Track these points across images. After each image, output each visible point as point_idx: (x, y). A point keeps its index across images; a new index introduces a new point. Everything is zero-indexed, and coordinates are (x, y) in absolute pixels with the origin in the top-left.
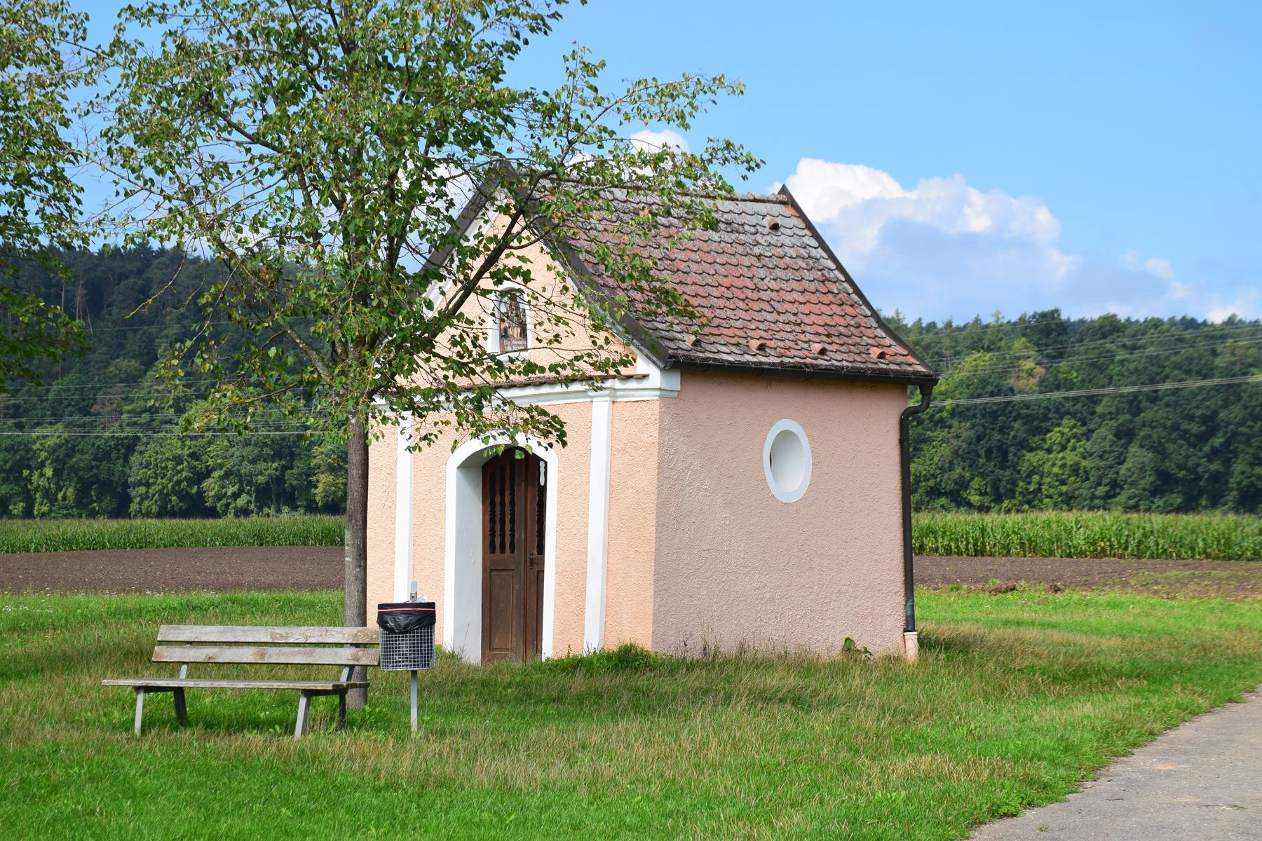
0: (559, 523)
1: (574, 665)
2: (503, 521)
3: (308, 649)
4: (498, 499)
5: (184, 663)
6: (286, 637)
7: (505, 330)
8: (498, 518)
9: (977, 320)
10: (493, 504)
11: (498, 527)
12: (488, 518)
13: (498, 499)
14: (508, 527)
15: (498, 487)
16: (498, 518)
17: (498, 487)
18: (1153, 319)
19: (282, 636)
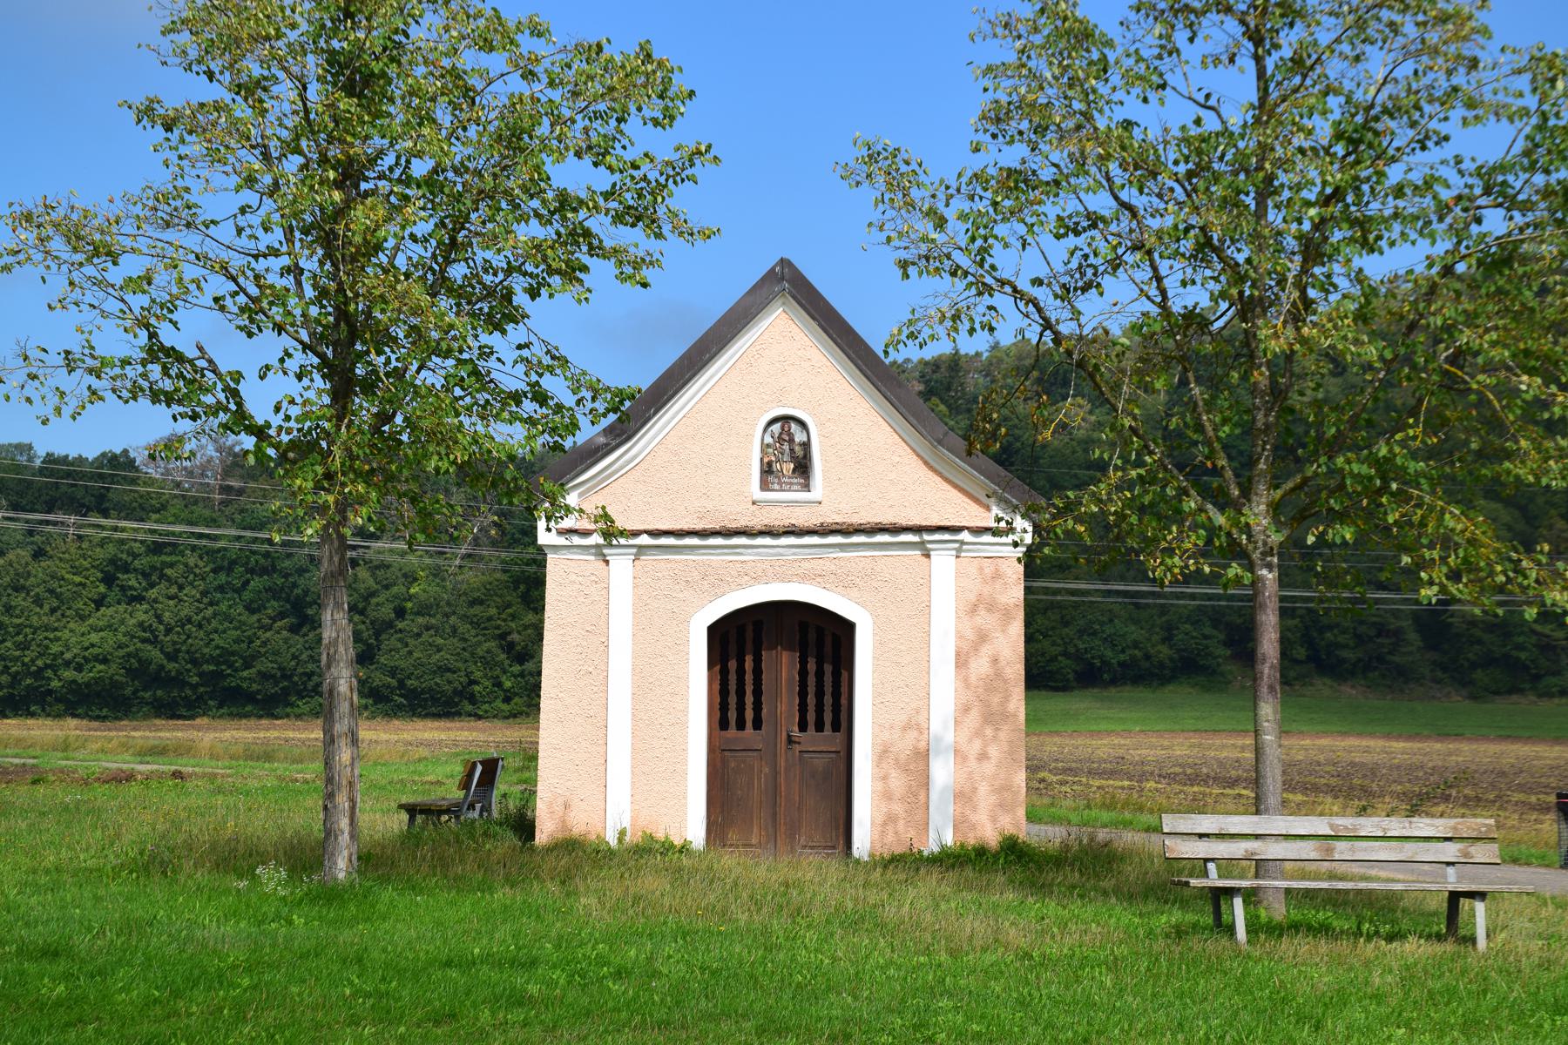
0: (877, 694)
1: (905, 863)
2: (820, 694)
3: (1394, 844)
4: (733, 665)
5: (1212, 860)
6: (1355, 830)
7: (770, 464)
8: (733, 687)
9: (125, 452)
10: (724, 673)
11: (733, 700)
12: (717, 687)
13: (733, 665)
14: (749, 699)
15: (733, 648)
16: (733, 687)
17: (733, 648)
18: (104, 455)
19: (1346, 828)
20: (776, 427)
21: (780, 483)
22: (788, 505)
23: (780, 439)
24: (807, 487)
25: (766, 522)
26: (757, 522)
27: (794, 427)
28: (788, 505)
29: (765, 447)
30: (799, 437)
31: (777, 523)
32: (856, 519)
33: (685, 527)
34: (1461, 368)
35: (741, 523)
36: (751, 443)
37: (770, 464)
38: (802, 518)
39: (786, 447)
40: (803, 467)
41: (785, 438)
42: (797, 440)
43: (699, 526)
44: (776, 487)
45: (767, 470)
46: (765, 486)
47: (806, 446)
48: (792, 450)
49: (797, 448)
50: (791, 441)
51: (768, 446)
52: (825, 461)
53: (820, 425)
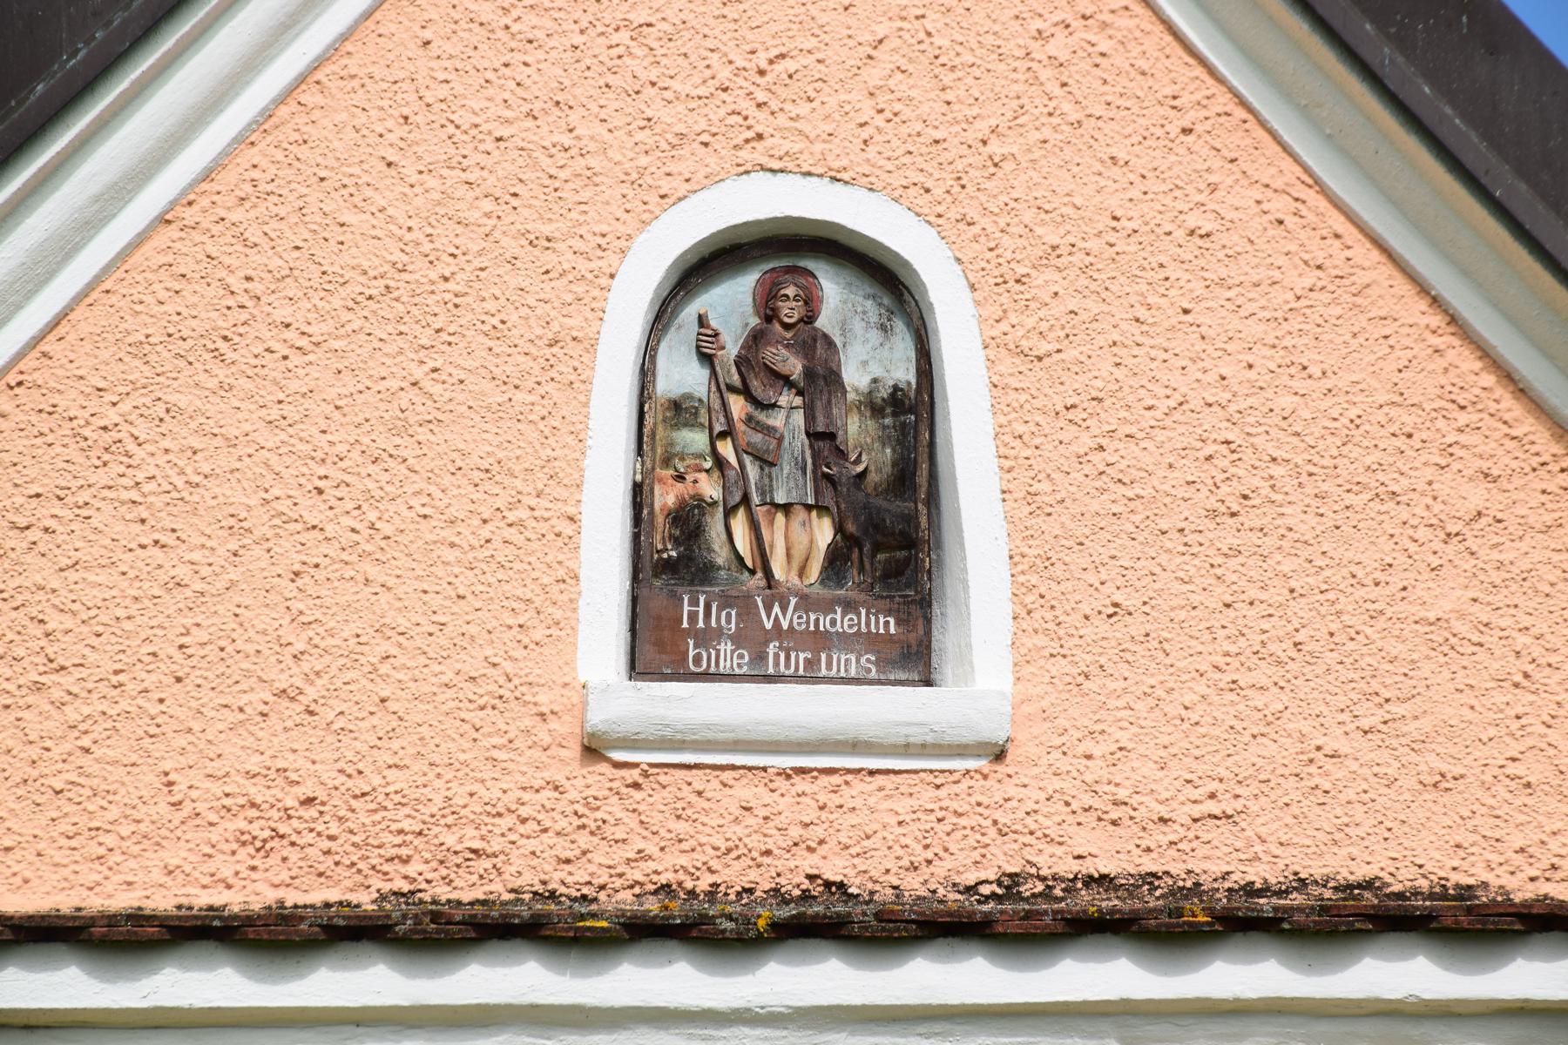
7: (688, 521)
20: (730, 302)
21: (753, 640)
22: (798, 756)
23: (752, 374)
24: (913, 659)
25: (667, 867)
26: (616, 862)
27: (837, 296)
28: (798, 756)
29: (656, 418)
30: (870, 360)
31: (734, 875)
32: (1220, 861)
33: (162, 902)
34: (795, 610)
35: (519, 871)
36: (580, 384)
37: (688, 521)
38: (881, 845)
39: (789, 418)
40: (891, 546)
41: (782, 363)
42: (855, 377)
43: (249, 892)
44: (728, 656)
45: (673, 562)
46: (655, 649)
47: (912, 412)
48: (823, 439)
49: (855, 429)
50: (821, 380)
51: (681, 411)
52: (1026, 500)
53: (998, 284)
